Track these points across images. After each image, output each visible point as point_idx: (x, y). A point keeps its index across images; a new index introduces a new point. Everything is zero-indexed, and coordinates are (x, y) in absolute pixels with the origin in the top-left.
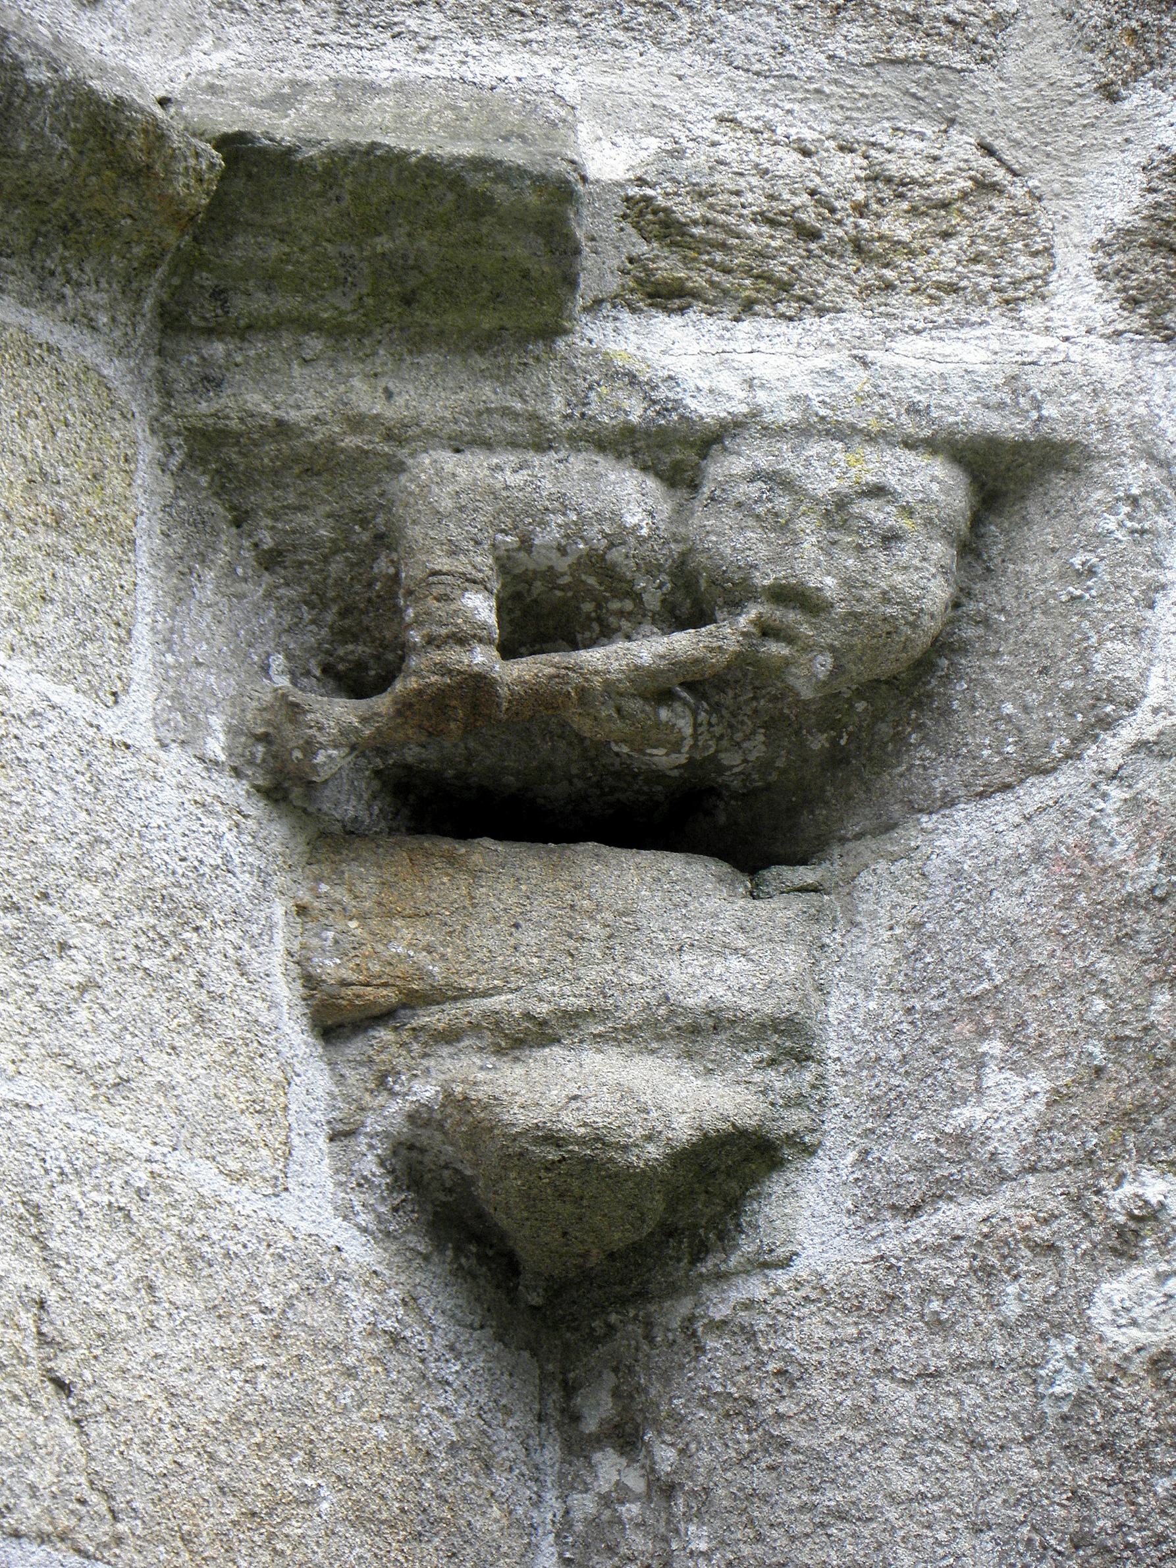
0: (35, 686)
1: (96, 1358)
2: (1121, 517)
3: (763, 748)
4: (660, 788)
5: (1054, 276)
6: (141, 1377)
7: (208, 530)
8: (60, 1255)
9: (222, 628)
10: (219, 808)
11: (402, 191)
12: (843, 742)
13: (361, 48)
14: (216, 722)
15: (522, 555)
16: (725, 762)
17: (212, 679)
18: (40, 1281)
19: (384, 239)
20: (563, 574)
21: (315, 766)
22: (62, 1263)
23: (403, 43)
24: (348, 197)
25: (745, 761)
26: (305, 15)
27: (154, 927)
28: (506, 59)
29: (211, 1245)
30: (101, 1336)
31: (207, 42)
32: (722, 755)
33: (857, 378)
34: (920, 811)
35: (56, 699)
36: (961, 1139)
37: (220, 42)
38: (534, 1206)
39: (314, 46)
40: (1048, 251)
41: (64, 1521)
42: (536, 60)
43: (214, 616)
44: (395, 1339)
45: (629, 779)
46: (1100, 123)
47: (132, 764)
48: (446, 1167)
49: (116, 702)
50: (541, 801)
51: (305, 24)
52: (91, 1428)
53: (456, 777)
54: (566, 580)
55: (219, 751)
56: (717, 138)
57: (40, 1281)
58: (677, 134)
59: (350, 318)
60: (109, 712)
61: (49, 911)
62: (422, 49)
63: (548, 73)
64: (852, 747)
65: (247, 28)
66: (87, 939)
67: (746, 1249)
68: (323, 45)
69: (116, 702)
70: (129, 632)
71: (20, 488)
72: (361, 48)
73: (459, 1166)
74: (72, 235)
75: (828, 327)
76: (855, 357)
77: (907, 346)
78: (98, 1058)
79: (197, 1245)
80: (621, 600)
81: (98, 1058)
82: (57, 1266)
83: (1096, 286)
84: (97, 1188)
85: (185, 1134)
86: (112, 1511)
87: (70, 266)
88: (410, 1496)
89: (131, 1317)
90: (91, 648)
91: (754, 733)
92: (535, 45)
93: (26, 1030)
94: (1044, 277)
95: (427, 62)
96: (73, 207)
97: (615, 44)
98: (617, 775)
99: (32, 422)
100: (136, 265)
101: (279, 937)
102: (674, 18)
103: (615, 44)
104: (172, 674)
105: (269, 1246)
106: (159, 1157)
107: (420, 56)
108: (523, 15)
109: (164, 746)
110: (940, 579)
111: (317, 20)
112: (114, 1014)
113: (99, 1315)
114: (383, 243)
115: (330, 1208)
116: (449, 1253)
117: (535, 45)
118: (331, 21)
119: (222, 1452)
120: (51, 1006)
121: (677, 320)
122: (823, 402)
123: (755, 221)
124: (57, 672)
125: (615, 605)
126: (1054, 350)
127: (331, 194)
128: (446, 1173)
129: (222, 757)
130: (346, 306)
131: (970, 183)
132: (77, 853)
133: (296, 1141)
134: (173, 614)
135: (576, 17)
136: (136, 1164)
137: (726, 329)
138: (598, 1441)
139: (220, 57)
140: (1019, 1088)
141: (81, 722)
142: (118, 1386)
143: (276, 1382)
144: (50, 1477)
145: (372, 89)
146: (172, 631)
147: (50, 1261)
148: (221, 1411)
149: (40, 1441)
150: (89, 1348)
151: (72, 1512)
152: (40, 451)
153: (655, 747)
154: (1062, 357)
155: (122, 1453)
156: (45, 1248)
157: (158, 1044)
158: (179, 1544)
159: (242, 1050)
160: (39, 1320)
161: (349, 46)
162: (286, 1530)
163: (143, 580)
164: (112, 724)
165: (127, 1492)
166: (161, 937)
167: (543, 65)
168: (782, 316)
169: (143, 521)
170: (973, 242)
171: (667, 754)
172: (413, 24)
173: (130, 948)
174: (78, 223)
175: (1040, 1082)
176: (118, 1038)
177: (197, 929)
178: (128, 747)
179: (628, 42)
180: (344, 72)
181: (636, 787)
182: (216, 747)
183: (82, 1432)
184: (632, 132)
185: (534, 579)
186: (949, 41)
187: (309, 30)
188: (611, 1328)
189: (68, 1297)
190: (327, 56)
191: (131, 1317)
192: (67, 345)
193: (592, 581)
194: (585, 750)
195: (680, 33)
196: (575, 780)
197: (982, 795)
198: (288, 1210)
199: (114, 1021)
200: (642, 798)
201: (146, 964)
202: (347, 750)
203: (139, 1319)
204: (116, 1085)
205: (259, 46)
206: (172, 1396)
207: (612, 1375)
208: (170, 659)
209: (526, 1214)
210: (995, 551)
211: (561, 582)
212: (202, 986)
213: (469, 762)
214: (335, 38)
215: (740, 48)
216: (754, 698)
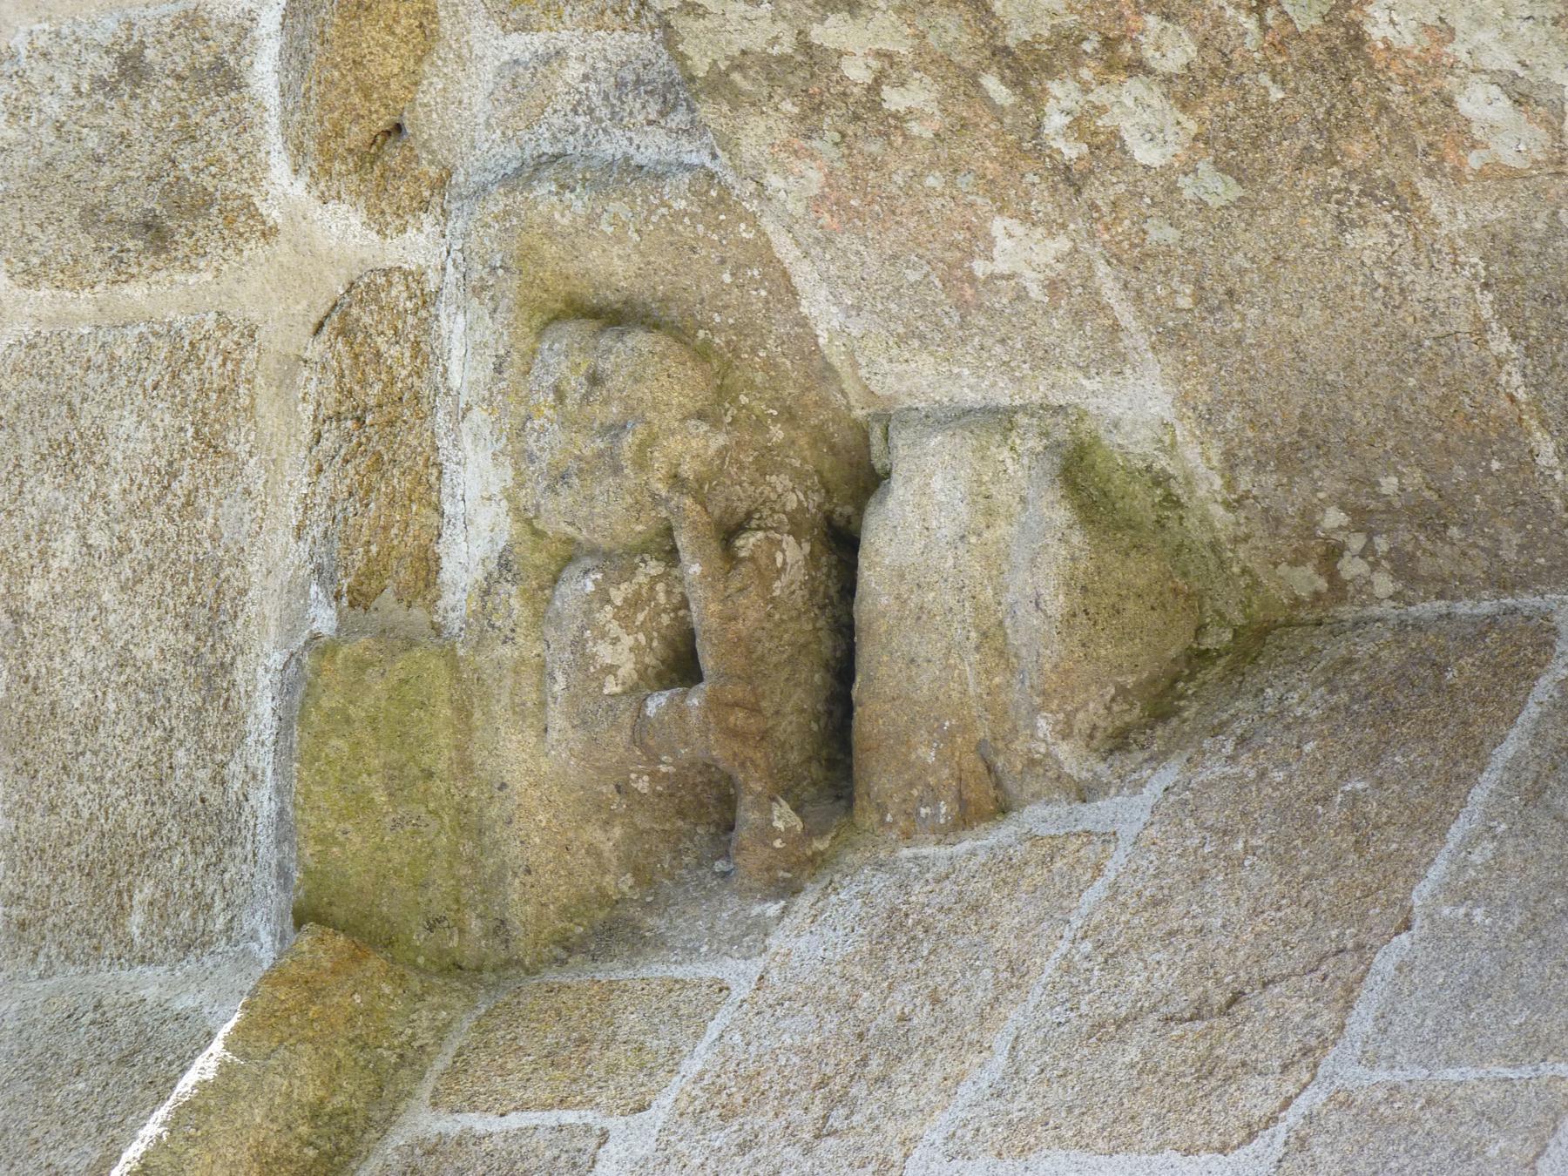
0: (703, 1052)
1: (1215, 973)
2: (573, 197)
3: (782, 476)
4: (824, 559)
5: (406, 266)
6: (1237, 937)
7: (615, 925)
8: (1134, 1007)
9: (689, 909)
10: (820, 904)
11: (332, 781)
12: (775, 413)
13: (255, 825)
14: (756, 910)
15: (621, 673)
16: (795, 505)
17: (724, 915)
18: (1151, 1021)
19: (374, 795)
20: (636, 640)
21: (786, 829)
22: (1139, 1004)
23: (251, 791)
24: (342, 825)
25: (793, 490)
26: (234, 870)
27: (899, 948)
28: (260, 710)
29: (1145, 888)
30: (1200, 971)
31: (255, 946)
32: (788, 508)
33: (477, 415)
34: (816, 344)
35: (715, 1035)
36: (1052, 287)
37: (254, 937)
38: (1129, 634)
39: (256, 862)
40: (387, 273)
41: (1338, 991)
42: (260, 687)
43: (680, 917)
44: (1242, 741)
45: (817, 583)
46: (294, 239)
47: (774, 973)
48: (1109, 709)
49: (728, 989)
50: (838, 654)
51: (240, 870)
52: (1270, 974)
53: (817, 721)
54: (641, 637)
55: (777, 907)
56: (310, 539)
57: (1151, 1021)
58: (308, 571)
59: (446, 819)
60: (734, 993)
61: (872, 1031)
62: (254, 777)
63: (269, 676)
64: (777, 404)
65: (244, 917)
66: (899, 1001)
67: (1164, 463)
68: (255, 855)
69: (728, 989)
70: (677, 981)
71: (556, 1072)
72: (255, 825)
73: (1108, 697)
74: (370, 1041)
75: (445, 441)
76: (463, 417)
77: (455, 381)
78: (989, 986)
79: (1144, 899)
80: (657, 593)
81: (989, 986)
82: (1142, 1007)
83: (411, 232)
84: (1087, 981)
85: (1058, 915)
86: (1336, 954)
87: (396, 1043)
88: (1362, 720)
89: (1190, 948)
90: (684, 1010)
91: (769, 484)
92: (249, 688)
93: (959, 1043)
94: (406, 274)
95: (264, 773)
96: (342, 1040)
97: (246, 625)
98: (813, 592)
99: (509, 1066)
100: (400, 991)
101: (925, 851)
102: (227, 580)
103: (246, 625)
104: (715, 947)
105: (1154, 844)
106: (1072, 934)
107: (260, 777)
108: (228, 699)
109: (765, 950)
110: (627, 338)
111: (237, 861)
112: (959, 975)
113: (1183, 974)
114: (380, 797)
115: (1134, 799)
116: (1182, 703)
117: (249, 688)
118: (238, 850)
119: (1305, 869)
120: (943, 1025)
121: (445, 562)
122: (497, 440)
123: (367, 505)
124: (697, 1036)
125: (662, 598)
126: (454, 260)
127: (341, 838)
128: (1116, 708)
129: (783, 903)
130: (435, 825)
131: (340, 338)
132: (833, 1012)
133: (1079, 828)
134: (673, 949)
135: (229, 657)
136: (1074, 951)
137: (449, 523)
138: (1333, 576)
139: (265, 938)
140: (1003, 243)
141: (736, 1015)
142: (1241, 954)
143: (1259, 831)
144: (1302, 1004)
145: (281, 813)
146: (684, 949)
147: (1134, 1017)
148: (1273, 872)
149: (1272, 1014)
150: (1208, 979)
151: (1331, 985)
152: (531, 1058)
153: (775, 560)
154: (460, 254)
155: (1292, 948)
156: (1126, 1020)
157: (987, 939)
158: (1369, 899)
159: (1003, 874)
160: (1182, 1021)
161: (254, 835)
162: (1373, 815)
163: (644, 972)
164: (741, 991)
165: (1323, 942)
166: (908, 942)
167: (264, 680)
168: (438, 478)
169: (598, 976)
170: (382, 333)
171: (783, 551)
172: (237, 785)
173: (913, 966)
174: (359, 1037)
175: (998, 226)
176: (977, 971)
177: (907, 915)
178: (762, 978)
179: (245, 616)
180: (272, 837)
181: (824, 578)
182: (773, 909)
183: (1272, 981)
184: (306, 607)
185: (643, 662)
186: (238, 363)
187: (244, 867)
188: (1244, 571)
189: (1166, 999)
190: (262, 851)
191: (1190, 948)
192: (457, 1044)
193: (641, 617)
194: (791, 619)
195: (237, 575)
196: (818, 625)
197: (795, 294)
198: (1127, 831)
199: (964, 976)
200: (834, 572)
201: (925, 953)
202: (774, 804)
203: (1193, 941)
204: (1013, 971)
205: (256, 906)
206: (1255, 912)
207: (1280, 567)
208: (704, 949)
209: (1137, 641)
210: (612, 298)
211: (644, 642)
212: (950, 909)
213: (803, 711)
214: (249, 847)
215: (246, 527)
216: (740, 485)
